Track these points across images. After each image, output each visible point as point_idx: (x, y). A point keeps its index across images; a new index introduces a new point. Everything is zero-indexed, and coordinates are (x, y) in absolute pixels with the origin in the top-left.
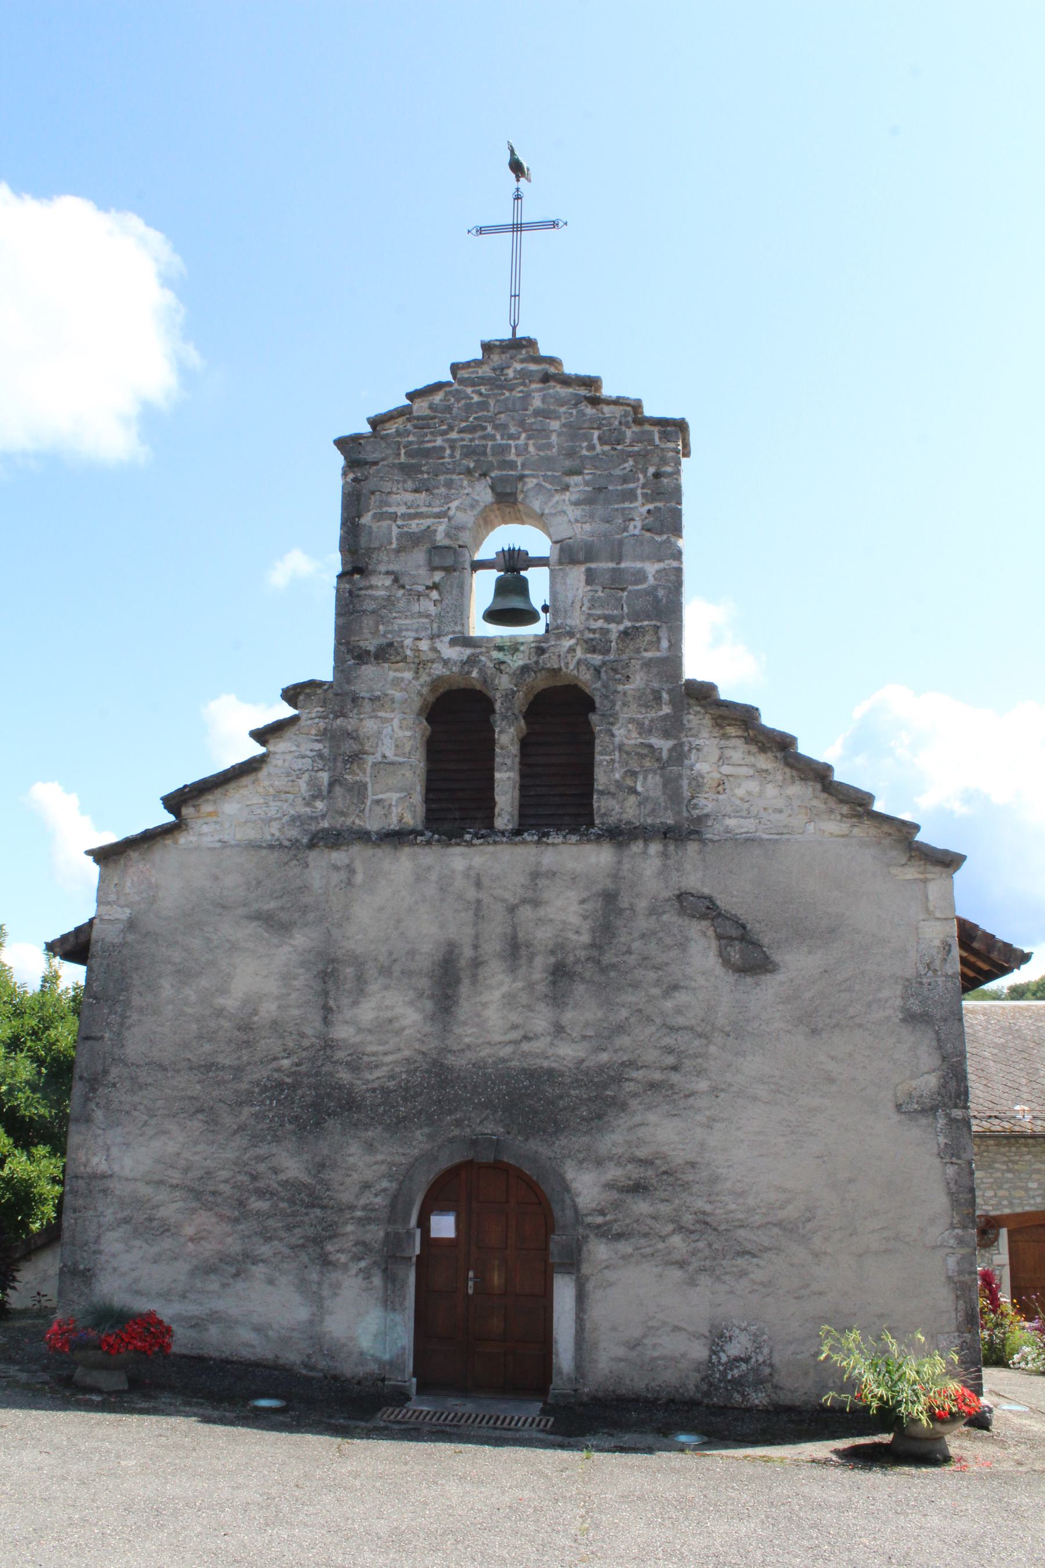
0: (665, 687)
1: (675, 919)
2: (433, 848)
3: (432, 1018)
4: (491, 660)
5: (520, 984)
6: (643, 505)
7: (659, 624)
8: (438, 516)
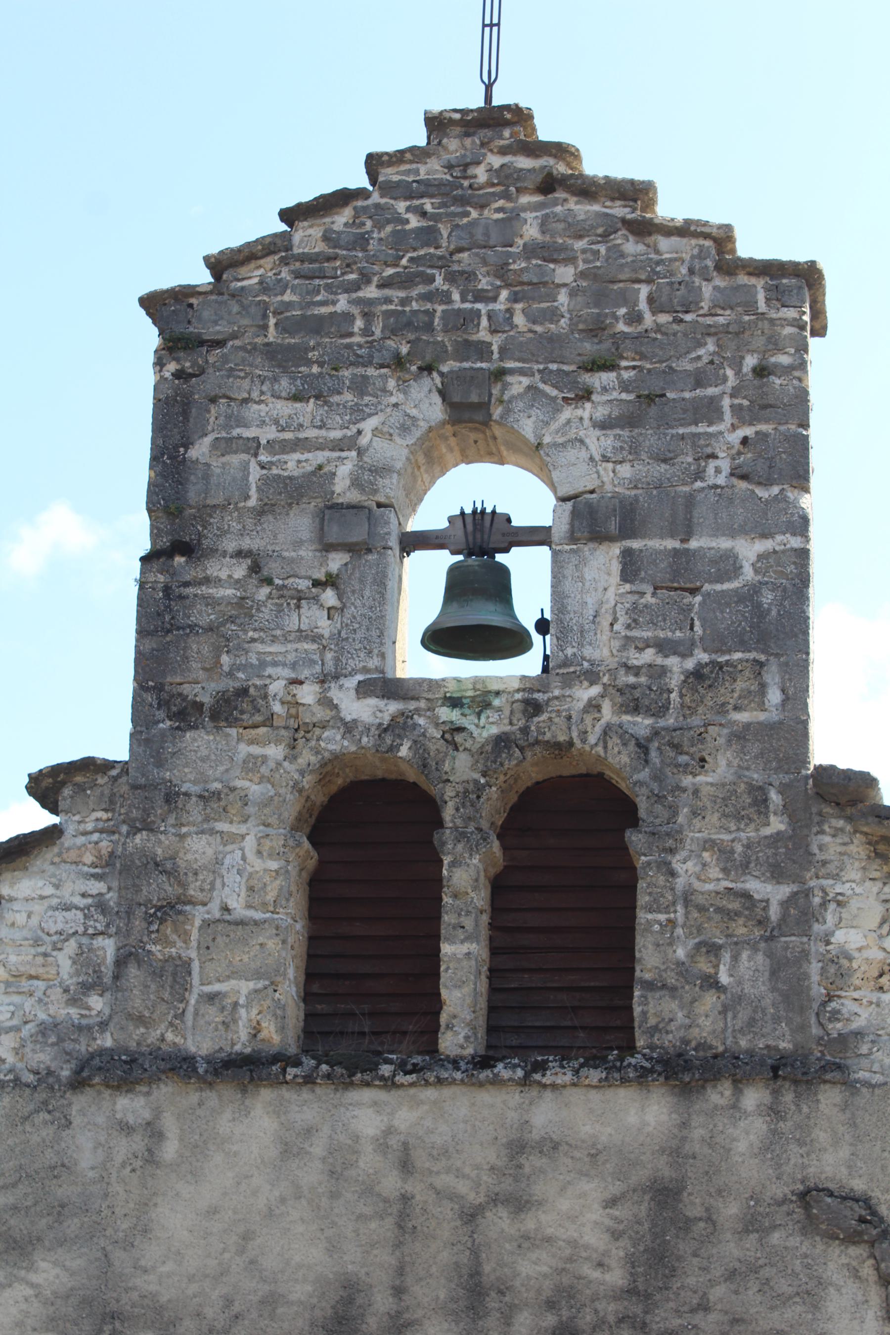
0: (776, 779)
1: (795, 1241)
2: (318, 1090)
7: (763, 658)
8: (339, 446)
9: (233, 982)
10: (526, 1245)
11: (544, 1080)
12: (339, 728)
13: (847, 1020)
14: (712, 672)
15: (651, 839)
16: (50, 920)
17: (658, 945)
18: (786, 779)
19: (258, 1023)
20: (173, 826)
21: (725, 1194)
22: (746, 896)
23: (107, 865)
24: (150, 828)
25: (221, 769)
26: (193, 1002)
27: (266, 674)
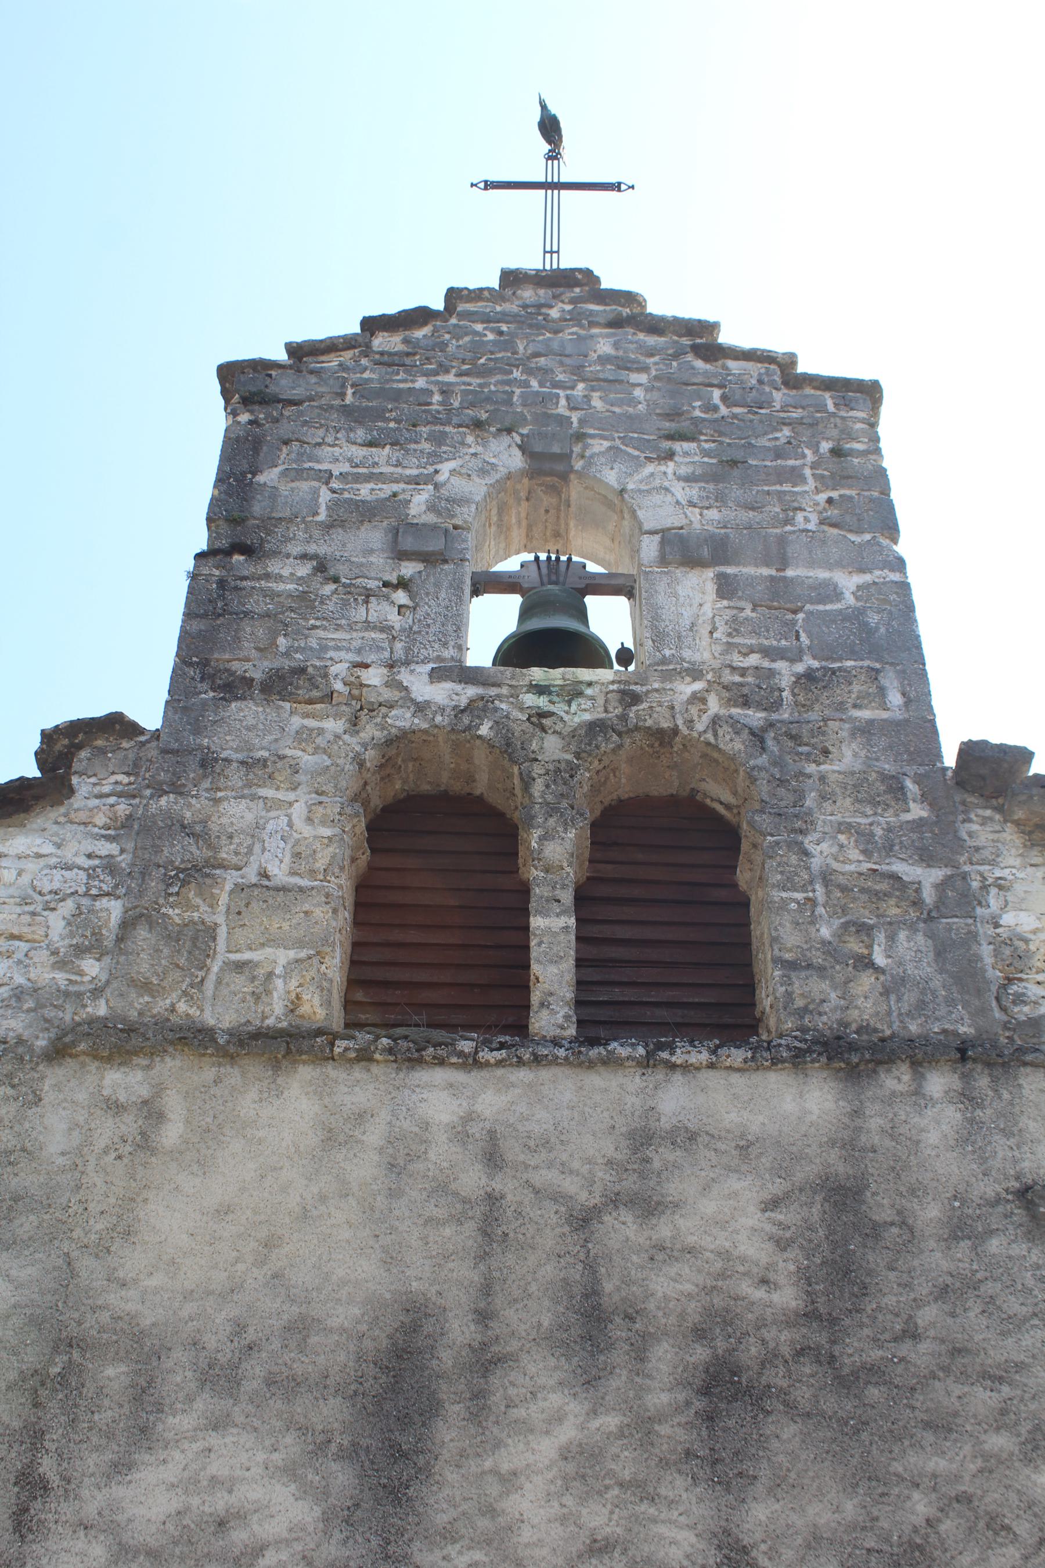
0: (911, 770)
1: (1019, 1249)
2: (375, 1069)
3: (345, 1518)
4: (522, 710)
5: (611, 1421)
6: (818, 491)
7: (878, 666)
8: (415, 481)
9: (268, 950)
10: (660, 1257)
11: (673, 1059)
12: (409, 708)
13: (1035, 1003)
14: (824, 676)
15: (777, 820)
16: (45, 879)
17: (798, 924)
18: (922, 770)
19: (298, 997)
20: (207, 790)
21: (920, 1193)
22: (895, 877)
23: (123, 827)
24: (178, 790)
25: (269, 738)
26: (215, 969)
27: (328, 656)
